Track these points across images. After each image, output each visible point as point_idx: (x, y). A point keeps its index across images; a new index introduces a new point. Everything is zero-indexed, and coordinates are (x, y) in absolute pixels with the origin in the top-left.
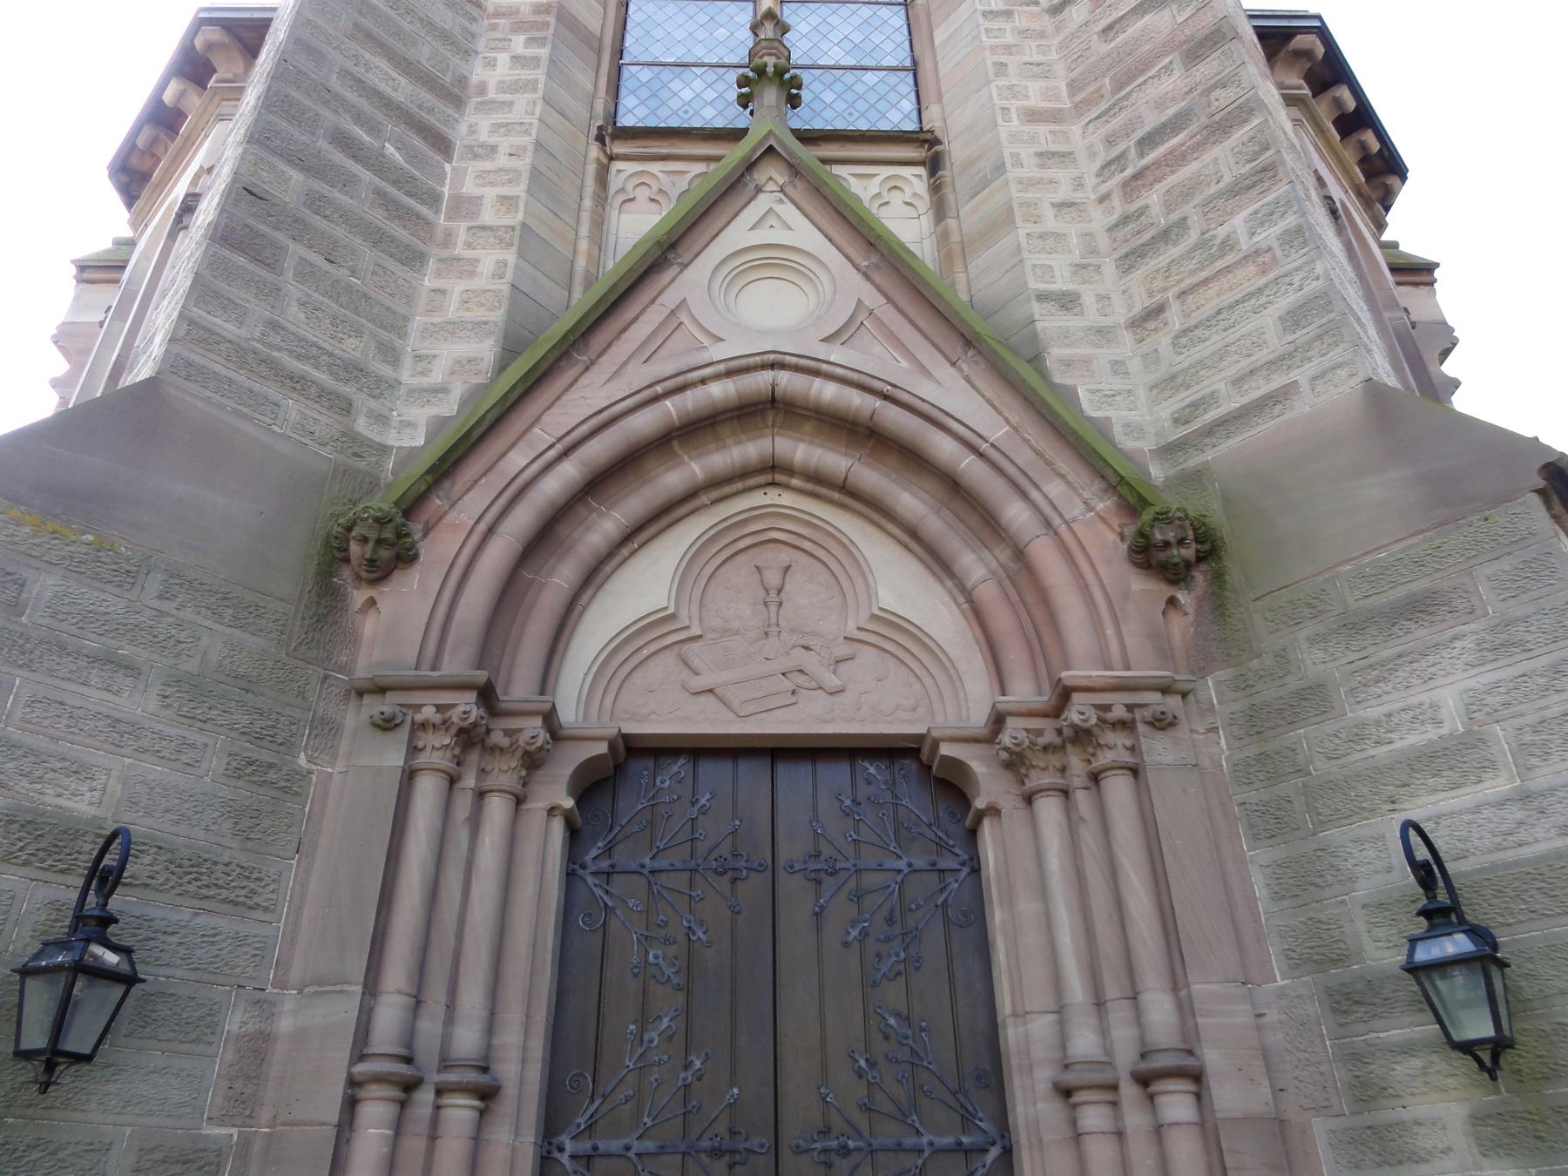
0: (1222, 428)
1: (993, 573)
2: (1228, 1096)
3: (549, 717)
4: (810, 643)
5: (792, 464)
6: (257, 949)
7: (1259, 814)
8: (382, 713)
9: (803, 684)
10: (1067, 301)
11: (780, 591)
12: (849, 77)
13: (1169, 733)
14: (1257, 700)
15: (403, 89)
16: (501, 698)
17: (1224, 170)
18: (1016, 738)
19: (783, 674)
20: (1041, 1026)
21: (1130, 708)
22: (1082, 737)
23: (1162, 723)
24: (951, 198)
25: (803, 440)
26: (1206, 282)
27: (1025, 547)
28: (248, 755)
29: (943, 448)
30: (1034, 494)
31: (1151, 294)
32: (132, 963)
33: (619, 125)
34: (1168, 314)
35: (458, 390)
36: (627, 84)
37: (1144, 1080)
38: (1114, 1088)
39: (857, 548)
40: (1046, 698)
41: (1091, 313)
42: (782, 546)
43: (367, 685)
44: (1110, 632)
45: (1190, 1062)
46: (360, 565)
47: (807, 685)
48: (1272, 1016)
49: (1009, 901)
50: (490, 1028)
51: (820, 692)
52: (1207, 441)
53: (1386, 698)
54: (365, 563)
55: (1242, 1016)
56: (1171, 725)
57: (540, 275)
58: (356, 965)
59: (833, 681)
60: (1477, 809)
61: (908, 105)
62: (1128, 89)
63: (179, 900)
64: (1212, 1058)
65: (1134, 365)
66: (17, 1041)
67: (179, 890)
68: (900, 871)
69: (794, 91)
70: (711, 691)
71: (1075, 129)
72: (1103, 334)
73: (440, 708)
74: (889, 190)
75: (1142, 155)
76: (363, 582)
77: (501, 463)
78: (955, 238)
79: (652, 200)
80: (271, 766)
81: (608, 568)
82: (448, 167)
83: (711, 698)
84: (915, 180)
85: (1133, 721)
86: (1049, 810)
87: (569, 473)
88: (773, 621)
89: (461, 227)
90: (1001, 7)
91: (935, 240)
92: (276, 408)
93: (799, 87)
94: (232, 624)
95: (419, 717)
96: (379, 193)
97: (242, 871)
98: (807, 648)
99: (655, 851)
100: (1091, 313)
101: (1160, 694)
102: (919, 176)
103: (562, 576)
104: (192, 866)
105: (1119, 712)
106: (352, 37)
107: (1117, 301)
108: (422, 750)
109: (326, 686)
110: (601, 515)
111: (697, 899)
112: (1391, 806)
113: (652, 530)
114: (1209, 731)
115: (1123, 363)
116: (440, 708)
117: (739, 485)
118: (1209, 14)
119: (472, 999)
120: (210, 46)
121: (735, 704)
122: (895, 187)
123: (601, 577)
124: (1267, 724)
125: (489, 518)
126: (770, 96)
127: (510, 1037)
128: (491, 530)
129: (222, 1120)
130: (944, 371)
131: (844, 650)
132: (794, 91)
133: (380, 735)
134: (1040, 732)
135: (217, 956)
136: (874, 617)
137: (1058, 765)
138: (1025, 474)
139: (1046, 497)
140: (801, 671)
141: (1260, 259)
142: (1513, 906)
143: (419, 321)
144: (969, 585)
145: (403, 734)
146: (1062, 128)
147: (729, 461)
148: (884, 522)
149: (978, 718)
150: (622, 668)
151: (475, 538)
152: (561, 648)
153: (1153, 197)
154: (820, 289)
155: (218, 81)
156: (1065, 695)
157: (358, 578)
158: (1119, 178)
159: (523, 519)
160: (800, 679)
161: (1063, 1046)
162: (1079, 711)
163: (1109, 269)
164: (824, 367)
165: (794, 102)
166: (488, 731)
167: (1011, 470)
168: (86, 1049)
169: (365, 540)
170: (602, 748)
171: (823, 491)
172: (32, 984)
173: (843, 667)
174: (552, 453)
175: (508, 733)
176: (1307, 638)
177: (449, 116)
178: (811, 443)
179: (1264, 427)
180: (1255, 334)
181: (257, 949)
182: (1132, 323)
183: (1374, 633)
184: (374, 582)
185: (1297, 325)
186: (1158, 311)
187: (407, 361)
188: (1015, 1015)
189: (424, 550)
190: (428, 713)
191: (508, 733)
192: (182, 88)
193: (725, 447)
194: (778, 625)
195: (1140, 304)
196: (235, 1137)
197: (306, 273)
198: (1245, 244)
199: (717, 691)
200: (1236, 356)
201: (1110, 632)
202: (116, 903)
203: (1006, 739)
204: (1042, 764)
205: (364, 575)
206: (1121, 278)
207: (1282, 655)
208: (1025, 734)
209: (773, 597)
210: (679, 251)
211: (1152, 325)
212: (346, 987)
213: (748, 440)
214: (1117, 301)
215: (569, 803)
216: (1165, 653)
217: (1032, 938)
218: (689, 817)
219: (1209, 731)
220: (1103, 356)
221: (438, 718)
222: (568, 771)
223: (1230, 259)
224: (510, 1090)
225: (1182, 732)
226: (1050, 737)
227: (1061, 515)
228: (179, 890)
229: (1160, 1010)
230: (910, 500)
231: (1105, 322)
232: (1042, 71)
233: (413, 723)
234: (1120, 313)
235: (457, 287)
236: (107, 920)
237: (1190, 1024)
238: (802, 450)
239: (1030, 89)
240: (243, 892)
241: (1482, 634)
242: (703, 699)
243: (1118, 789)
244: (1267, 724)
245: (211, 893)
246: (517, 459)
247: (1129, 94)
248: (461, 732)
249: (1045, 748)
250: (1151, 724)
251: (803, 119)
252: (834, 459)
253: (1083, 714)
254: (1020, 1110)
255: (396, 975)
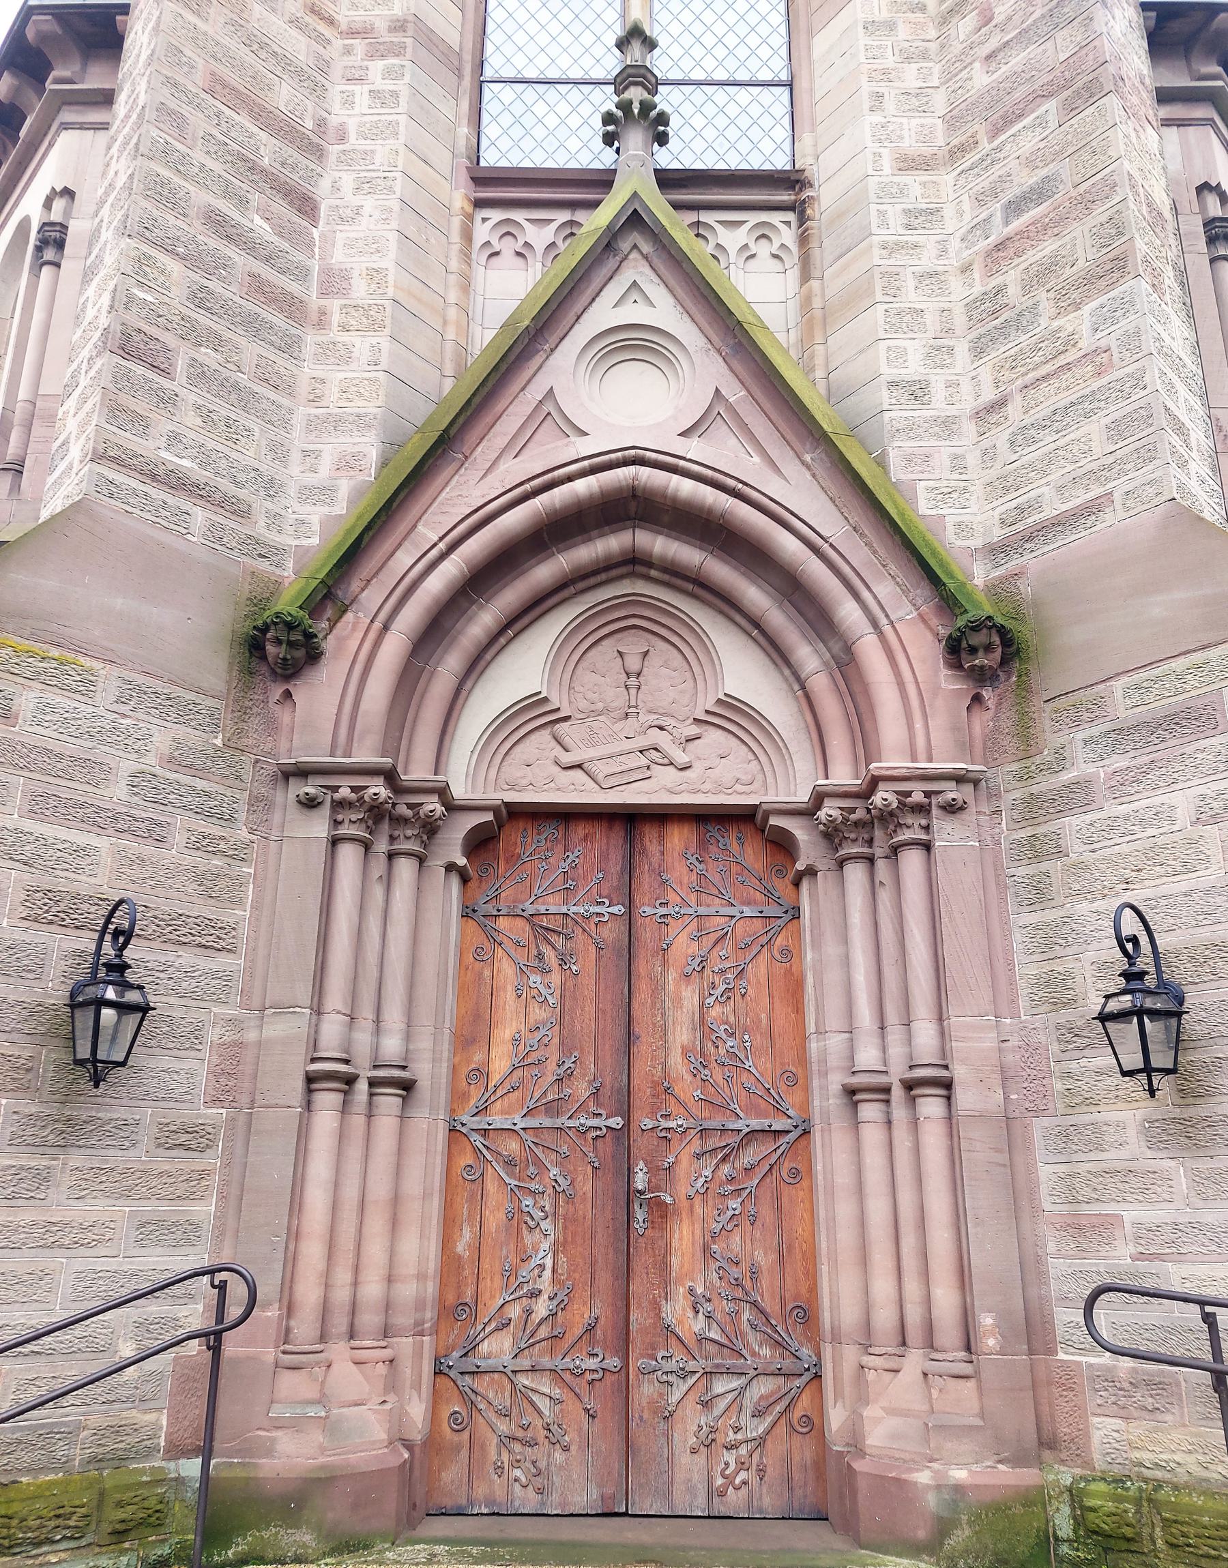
0: (1041, 533)
1: (826, 664)
2: (965, 1098)
3: (442, 792)
4: (663, 724)
5: (651, 556)
6: (226, 981)
7: (1023, 885)
8: (307, 794)
9: (658, 760)
10: (918, 392)
11: (639, 675)
12: (720, 95)
13: (958, 815)
14: (1035, 789)
15: (268, 149)
16: (403, 777)
17: (1080, 253)
18: (831, 816)
19: (641, 752)
20: (836, 1042)
21: (927, 794)
22: (887, 818)
23: (952, 809)
24: (816, 253)
25: (662, 534)
26: (1045, 378)
27: (854, 643)
28: (203, 830)
29: (788, 545)
30: (866, 594)
31: (997, 384)
32: (144, 997)
33: (483, 163)
34: (1010, 408)
35: (345, 488)
36: (488, 107)
37: (909, 1085)
38: (887, 1090)
39: (708, 636)
40: (859, 782)
41: (939, 404)
42: (641, 632)
43: (292, 769)
44: (919, 726)
45: (944, 1073)
46: (276, 663)
47: (661, 761)
48: (1014, 1042)
49: (817, 945)
50: (408, 1037)
51: (671, 768)
52: (1027, 546)
53: (1136, 797)
54: (279, 661)
55: (989, 1041)
56: (962, 809)
57: (414, 358)
58: (303, 992)
59: (681, 758)
60: (1187, 894)
61: (782, 133)
62: (1002, 138)
63: (164, 946)
64: (959, 1072)
65: (973, 460)
66: (75, 1056)
67: (163, 939)
68: (733, 917)
69: (661, 128)
70: (579, 766)
71: (947, 179)
72: (947, 426)
73: (354, 789)
74: (757, 239)
75: (1007, 223)
76: (278, 678)
77: (391, 563)
78: (817, 303)
79: (518, 254)
80: (222, 838)
81: (488, 657)
82: (316, 233)
83: (578, 774)
84: (782, 227)
85: (930, 804)
86: (855, 874)
87: (451, 570)
88: (633, 703)
89: (334, 306)
90: (885, 15)
91: (798, 302)
92: (187, 516)
93: (667, 124)
94: (176, 720)
95: (337, 796)
96: (254, 277)
97: (208, 922)
98: (661, 728)
99: (533, 898)
100: (939, 404)
101: (954, 783)
102: (788, 223)
103: (451, 663)
104: (171, 920)
105: (918, 797)
106: (211, 92)
107: (966, 387)
108: (340, 823)
109: (258, 769)
110: (481, 607)
111: (563, 1156)
112: (1125, 886)
113: (526, 620)
114: (994, 812)
115: (963, 457)
116: (354, 789)
117: (603, 576)
118: (1091, 57)
119: (394, 1016)
120: (43, 37)
121: (600, 777)
122: (763, 236)
123: (483, 663)
124: (1040, 812)
125: (383, 616)
126: (635, 139)
127: (424, 1043)
128: (386, 627)
129: (215, 1102)
130: (791, 467)
131: (694, 730)
132: (661, 128)
133: (305, 811)
134: (853, 810)
135: (197, 987)
136: (719, 701)
137: (866, 836)
138: (858, 574)
139: (875, 597)
140: (656, 749)
141: (1098, 359)
142: (1200, 969)
143: (302, 413)
144: (803, 676)
145: (326, 810)
146: (934, 178)
147: (594, 555)
148: (733, 613)
149: (802, 796)
150: (503, 745)
151: (372, 636)
152: (450, 729)
153: (1012, 278)
154: (681, 375)
155: (58, 81)
156: (874, 783)
157: (274, 672)
158: (984, 245)
159: (412, 615)
160: (654, 755)
161: (852, 1058)
162: (884, 796)
163: (962, 349)
164: (682, 463)
165: (662, 139)
166: (394, 805)
167: (846, 570)
168: (120, 1057)
169: (278, 642)
170: (489, 817)
171: (679, 582)
172: (78, 1013)
173: (691, 745)
174: (434, 553)
175: (410, 806)
176: (1084, 740)
177: (312, 170)
178: (668, 536)
179: (1080, 540)
180: (1083, 440)
181: (226, 981)
182: (977, 413)
183: (1137, 739)
184: (288, 678)
185: (1121, 436)
186: (1000, 404)
187: (296, 456)
188: (818, 1032)
189: (329, 645)
190: (345, 792)
191: (410, 806)
192: (16, 83)
193: (590, 540)
194: (636, 707)
195: (989, 395)
196: (224, 1115)
197: (199, 375)
198: (1086, 342)
199: (585, 766)
200: (1063, 461)
201: (919, 726)
202: (129, 954)
203: (822, 814)
204: (853, 836)
205: (279, 671)
206: (973, 362)
207: (1060, 754)
208: (840, 812)
209: (633, 678)
210: (546, 335)
211: (994, 418)
212: (297, 1010)
213: (612, 533)
214: (966, 387)
215: (462, 861)
216: (965, 747)
217: (833, 977)
218: (561, 870)
219: (994, 812)
220: (944, 451)
221: (353, 796)
222: (462, 835)
223: (1071, 356)
224: (424, 1084)
225: (970, 816)
226: (860, 814)
227: (887, 616)
228: (163, 939)
229: (925, 1034)
230: (754, 595)
231: (952, 411)
232: (917, 100)
233: (333, 801)
234: (968, 403)
235: (336, 377)
236: (122, 968)
237: (948, 1047)
238: (661, 545)
239: (906, 127)
240: (211, 938)
241: (1219, 747)
242: (571, 773)
243: (912, 861)
244: (1040, 812)
245: (187, 941)
246: (404, 559)
247: (1003, 144)
248: (371, 809)
249: (856, 824)
250: (943, 808)
251: (666, 158)
252: (687, 554)
253: (886, 800)
254: (816, 1103)
255: (335, 999)
